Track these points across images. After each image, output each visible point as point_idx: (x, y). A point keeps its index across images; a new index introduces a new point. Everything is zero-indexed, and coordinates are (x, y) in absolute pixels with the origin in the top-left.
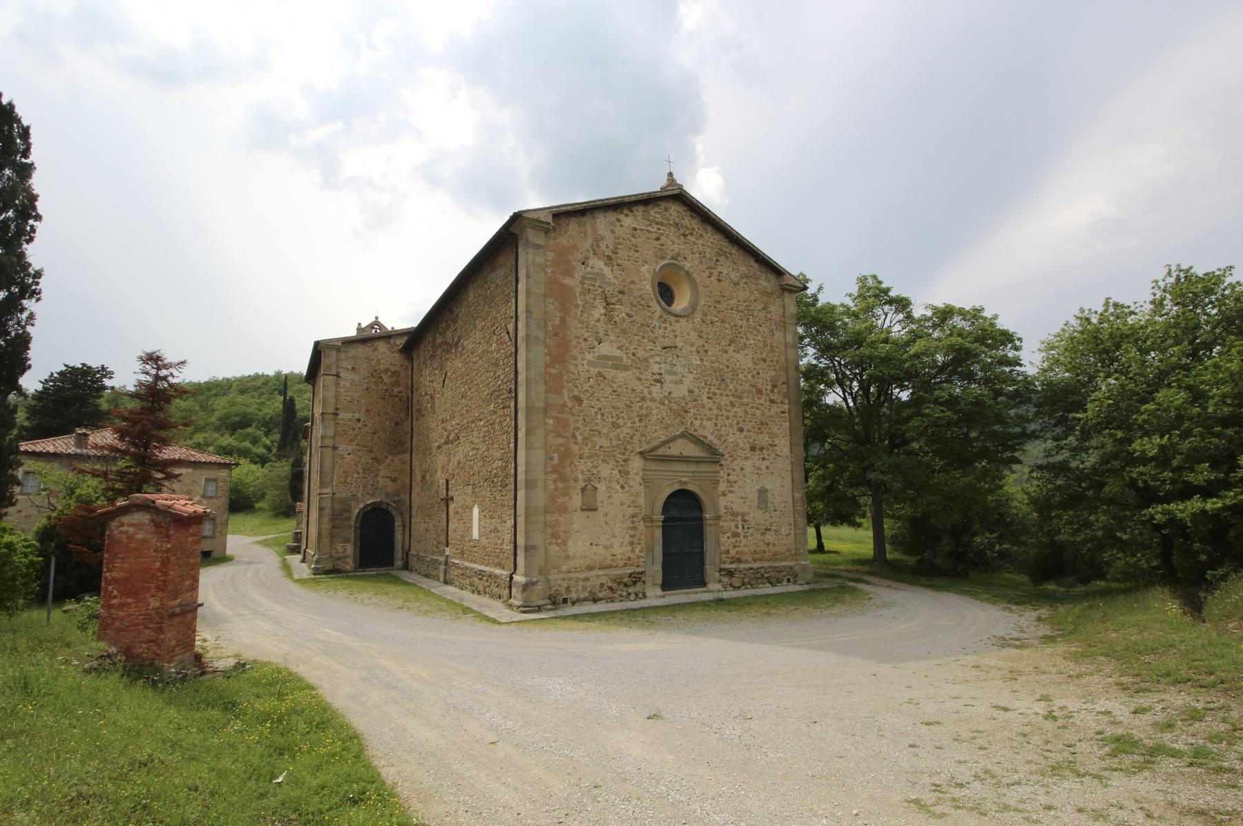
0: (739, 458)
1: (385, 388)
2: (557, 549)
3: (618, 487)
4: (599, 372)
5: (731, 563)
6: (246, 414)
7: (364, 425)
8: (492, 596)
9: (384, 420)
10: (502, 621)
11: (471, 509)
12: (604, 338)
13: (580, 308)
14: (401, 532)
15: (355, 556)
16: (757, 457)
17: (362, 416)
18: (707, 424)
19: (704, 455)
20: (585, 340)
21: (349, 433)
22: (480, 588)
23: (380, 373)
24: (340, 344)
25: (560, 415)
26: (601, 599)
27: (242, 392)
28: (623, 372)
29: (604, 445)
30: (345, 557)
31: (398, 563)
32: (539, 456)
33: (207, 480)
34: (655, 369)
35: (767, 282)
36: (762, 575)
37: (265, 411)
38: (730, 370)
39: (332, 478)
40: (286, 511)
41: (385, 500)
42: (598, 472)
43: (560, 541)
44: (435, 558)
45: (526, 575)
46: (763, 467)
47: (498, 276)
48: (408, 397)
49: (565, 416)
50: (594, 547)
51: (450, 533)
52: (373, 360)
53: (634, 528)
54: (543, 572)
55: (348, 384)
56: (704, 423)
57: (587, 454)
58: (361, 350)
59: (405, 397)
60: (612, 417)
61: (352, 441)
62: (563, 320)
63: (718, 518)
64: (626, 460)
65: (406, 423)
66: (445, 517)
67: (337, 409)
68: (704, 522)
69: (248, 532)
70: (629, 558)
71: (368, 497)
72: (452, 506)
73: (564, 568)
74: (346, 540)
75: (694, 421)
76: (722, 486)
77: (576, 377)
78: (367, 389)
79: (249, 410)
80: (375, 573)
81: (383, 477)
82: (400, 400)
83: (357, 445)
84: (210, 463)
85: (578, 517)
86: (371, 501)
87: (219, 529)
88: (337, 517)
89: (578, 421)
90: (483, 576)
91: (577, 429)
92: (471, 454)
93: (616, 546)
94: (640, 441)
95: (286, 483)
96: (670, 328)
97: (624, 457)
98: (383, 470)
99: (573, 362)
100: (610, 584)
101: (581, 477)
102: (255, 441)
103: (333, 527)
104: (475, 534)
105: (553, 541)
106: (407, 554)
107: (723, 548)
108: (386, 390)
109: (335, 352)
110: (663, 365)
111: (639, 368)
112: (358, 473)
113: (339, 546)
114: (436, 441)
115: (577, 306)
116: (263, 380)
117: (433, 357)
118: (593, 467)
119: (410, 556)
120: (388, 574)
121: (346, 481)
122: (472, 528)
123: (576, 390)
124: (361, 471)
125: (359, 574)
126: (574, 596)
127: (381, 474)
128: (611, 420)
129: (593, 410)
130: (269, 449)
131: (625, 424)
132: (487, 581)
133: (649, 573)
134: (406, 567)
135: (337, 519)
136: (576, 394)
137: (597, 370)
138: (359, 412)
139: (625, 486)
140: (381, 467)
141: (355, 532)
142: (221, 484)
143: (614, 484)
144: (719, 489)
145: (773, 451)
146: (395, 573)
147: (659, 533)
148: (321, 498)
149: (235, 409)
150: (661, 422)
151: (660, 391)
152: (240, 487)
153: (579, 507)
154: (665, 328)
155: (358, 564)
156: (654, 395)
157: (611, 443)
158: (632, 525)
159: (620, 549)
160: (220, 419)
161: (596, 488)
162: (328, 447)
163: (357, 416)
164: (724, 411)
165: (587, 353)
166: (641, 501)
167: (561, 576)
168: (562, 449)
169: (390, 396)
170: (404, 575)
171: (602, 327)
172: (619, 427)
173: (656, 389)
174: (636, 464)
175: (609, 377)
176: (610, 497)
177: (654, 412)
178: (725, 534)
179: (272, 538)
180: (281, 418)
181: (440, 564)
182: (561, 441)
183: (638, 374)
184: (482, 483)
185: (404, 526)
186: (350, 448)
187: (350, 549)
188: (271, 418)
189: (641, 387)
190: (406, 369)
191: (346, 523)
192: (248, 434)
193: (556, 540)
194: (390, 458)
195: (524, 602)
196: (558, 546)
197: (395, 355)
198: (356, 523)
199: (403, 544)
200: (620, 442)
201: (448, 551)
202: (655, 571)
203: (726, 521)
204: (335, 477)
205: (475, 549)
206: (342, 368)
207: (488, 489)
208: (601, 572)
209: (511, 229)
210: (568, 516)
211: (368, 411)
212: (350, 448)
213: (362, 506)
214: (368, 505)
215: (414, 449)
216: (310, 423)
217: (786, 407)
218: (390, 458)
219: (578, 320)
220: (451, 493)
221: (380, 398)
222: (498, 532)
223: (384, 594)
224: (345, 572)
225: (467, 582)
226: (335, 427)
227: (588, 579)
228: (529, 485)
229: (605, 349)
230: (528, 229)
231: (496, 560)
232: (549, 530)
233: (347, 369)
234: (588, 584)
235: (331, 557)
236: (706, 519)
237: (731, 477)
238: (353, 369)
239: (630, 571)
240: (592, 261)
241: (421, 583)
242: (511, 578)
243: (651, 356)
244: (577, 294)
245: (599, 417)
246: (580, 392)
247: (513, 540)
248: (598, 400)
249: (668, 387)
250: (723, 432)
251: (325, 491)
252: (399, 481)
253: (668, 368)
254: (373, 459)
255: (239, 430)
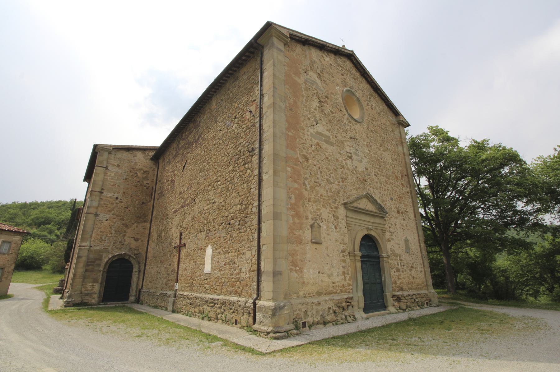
0: (393, 217)
1: (138, 180)
2: (296, 275)
3: (333, 227)
4: (317, 142)
5: (398, 291)
6: (49, 218)
7: (120, 202)
8: (226, 322)
9: (135, 200)
10: (263, 350)
11: (203, 250)
12: (319, 122)
13: (305, 98)
14: (137, 276)
15: (100, 292)
16: (401, 218)
17: (120, 195)
18: (376, 191)
19: (377, 211)
20: (309, 119)
21: (109, 206)
22: (211, 315)
23: (136, 170)
24: (112, 148)
25: (295, 166)
26: (329, 322)
27: (49, 208)
28: (331, 146)
29: (324, 195)
30: (92, 294)
31: (132, 298)
32: (282, 194)
33: (4, 242)
34: (348, 149)
35: (391, 117)
36: (415, 300)
37: (60, 217)
38: (382, 161)
39: (92, 235)
40: (60, 270)
41: (128, 253)
42: (321, 214)
43: (298, 268)
44: (165, 292)
45: (274, 299)
46: (405, 225)
47: (244, 75)
48: (153, 188)
49: (298, 167)
50: (321, 275)
51: (180, 272)
52: (132, 162)
53: (344, 261)
54: (287, 296)
55: (113, 175)
56: (375, 191)
57: (313, 199)
58: (125, 154)
59: (151, 187)
60: (327, 176)
61: (110, 211)
62: (295, 102)
63: (388, 257)
64: (336, 208)
65: (149, 203)
66: (177, 260)
67: (103, 189)
68: (381, 259)
69: (32, 282)
70: (343, 285)
71: (116, 250)
72: (184, 251)
73: (301, 293)
74: (95, 281)
75: (370, 188)
76: (388, 235)
77: (304, 141)
78: (126, 179)
79: (50, 216)
80: (114, 305)
81: (129, 237)
82: (147, 188)
83: (113, 214)
84: (8, 230)
85: (310, 248)
86: (117, 254)
87: (6, 276)
88: (90, 264)
89: (306, 173)
90: (215, 304)
91: (306, 179)
92: (206, 208)
93: (335, 274)
94: (343, 195)
95: (63, 254)
96: (353, 127)
97: (335, 205)
98: (130, 232)
99: (302, 131)
100: (334, 308)
101: (310, 216)
102: (51, 232)
103: (86, 271)
104: (208, 268)
105: (293, 268)
106: (140, 291)
107: (393, 279)
108: (138, 181)
109: (108, 153)
110: (351, 148)
111: (339, 146)
112: (111, 233)
113: (89, 286)
114: (173, 208)
115: (303, 96)
116: (63, 203)
117: (176, 156)
118: (317, 209)
119: (142, 293)
120: (124, 306)
121: (101, 238)
122: (204, 264)
123: (304, 151)
124: (113, 232)
125: (101, 306)
126: (310, 320)
127: (128, 235)
128: (326, 177)
129: (315, 168)
130: (57, 236)
131: (334, 182)
132: (220, 308)
133: (356, 299)
134: (138, 301)
135: (89, 265)
136: (305, 154)
137: (316, 141)
138: (118, 193)
139: (338, 227)
140: (128, 231)
141: (102, 275)
142: (13, 245)
143: (331, 224)
144: (386, 237)
145: (407, 215)
146: (129, 305)
147: (359, 265)
148: (80, 249)
149: (42, 215)
150: (354, 185)
151: (351, 164)
152: (34, 256)
153: (309, 240)
154: (351, 126)
155: (101, 299)
156: (349, 166)
157: (327, 194)
158: (343, 258)
159: (338, 279)
160: (33, 219)
161: (320, 226)
162: (92, 214)
163: (116, 195)
164: (383, 186)
165: (310, 128)
166: (347, 240)
167: (300, 301)
168: (297, 192)
169: (141, 185)
170: (136, 307)
171: (318, 114)
172: (331, 183)
173: (349, 162)
174: (342, 211)
175: (323, 147)
176: (329, 235)
177: (350, 177)
178: (392, 269)
179: (46, 285)
180: (68, 221)
181: (169, 296)
182: (296, 186)
183: (339, 150)
184: (217, 227)
185: (140, 271)
186: (108, 216)
187: (97, 287)
188: (63, 221)
189: (341, 159)
190: (154, 170)
191: (96, 268)
192: (47, 229)
193: (295, 267)
194: (135, 224)
195: (274, 327)
196: (297, 273)
197: (147, 161)
198: (104, 269)
199: (137, 284)
200: (332, 194)
201: (177, 286)
202: (359, 296)
203: (392, 260)
204: (94, 235)
205: (206, 282)
206: (111, 164)
207: (224, 230)
208: (327, 298)
209: (259, 41)
210: (302, 247)
211: (124, 193)
212: (108, 216)
213: (111, 256)
214: (115, 256)
215: (153, 219)
216: (82, 207)
217: (409, 189)
218: (135, 224)
219: (304, 105)
220: (183, 242)
221: (133, 186)
222: (234, 263)
223: (121, 322)
224: (91, 305)
225: (197, 310)
226: (99, 201)
227: (320, 304)
228: (276, 216)
229: (320, 128)
230: (274, 38)
231: (231, 289)
232: (290, 258)
233: (114, 165)
234: (320, 308)
235: (81, 293)
236: (383, 257)
237: (391, 229)
238: (118, 166)
239: (346, 297)
240: (310, 73)
241: (153, 312)
242: (255, 304)
243: (345, 141)
244: (303, 89)
245: (319, 173)
246: (307, 153)
247: (255, 267)
248: (318, 161)
249: (355, 163)
250: (384, 199)
251: (84, 244)
252: (139, 241)
253: (354, 150)
254: (123, 224)
255: (42, 226)
